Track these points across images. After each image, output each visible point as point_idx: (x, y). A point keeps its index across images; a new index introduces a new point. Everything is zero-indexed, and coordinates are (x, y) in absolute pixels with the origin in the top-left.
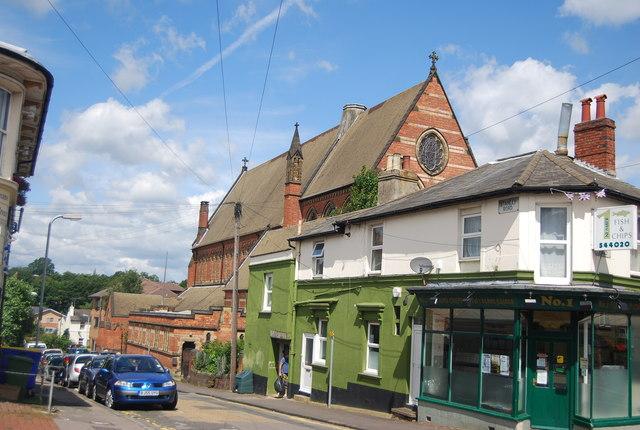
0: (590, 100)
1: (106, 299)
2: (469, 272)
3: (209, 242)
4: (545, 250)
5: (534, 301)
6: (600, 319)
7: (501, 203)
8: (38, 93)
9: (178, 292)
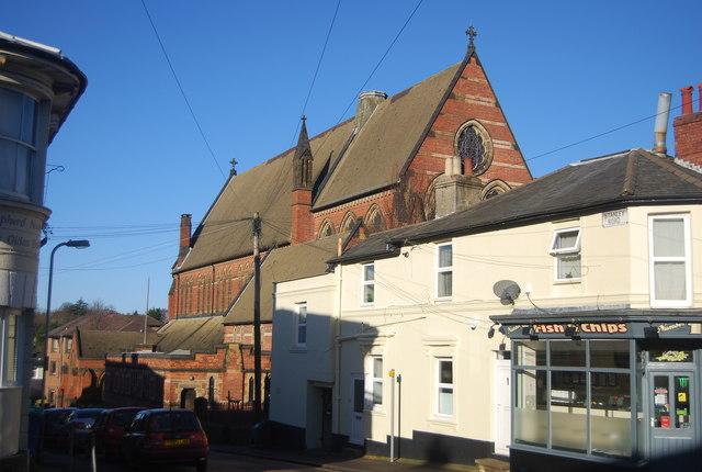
2: (261, 305)
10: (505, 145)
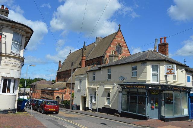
1: (35, 85)
3: (61, 71)
4: (153, 75)
5: (151, 87)
6: (167, 92)
7: (142, 63)
8: (29, 35)
9: (53, 84)
10: (126, 49)
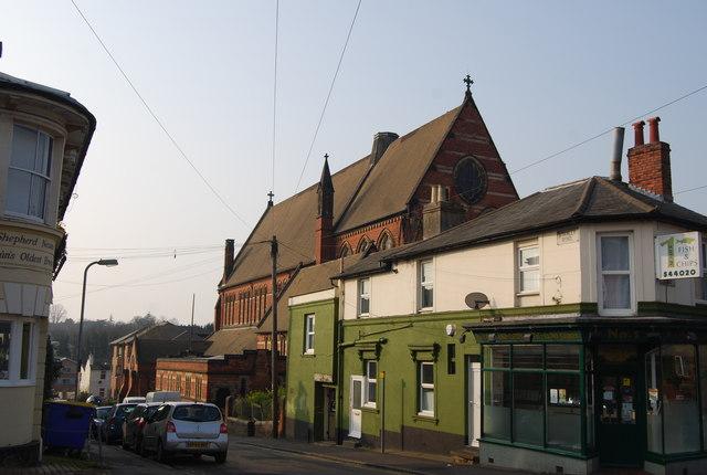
0: (643, 123)
8: (79, 136)
